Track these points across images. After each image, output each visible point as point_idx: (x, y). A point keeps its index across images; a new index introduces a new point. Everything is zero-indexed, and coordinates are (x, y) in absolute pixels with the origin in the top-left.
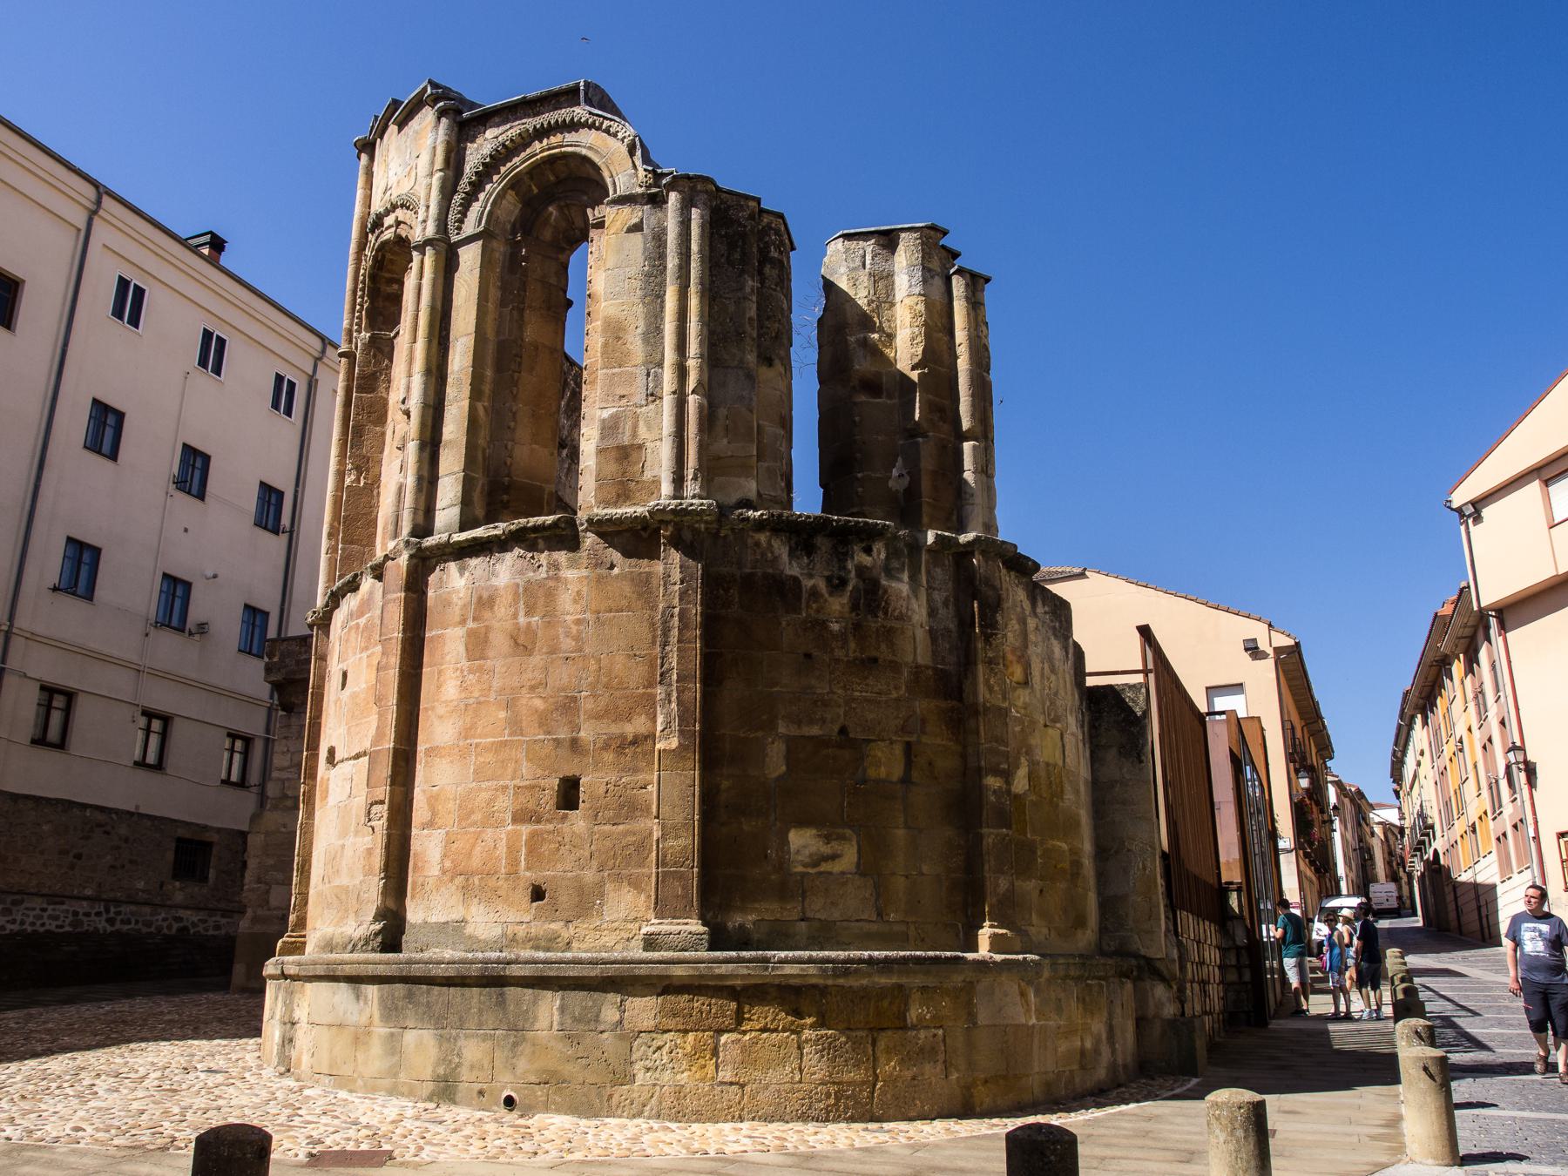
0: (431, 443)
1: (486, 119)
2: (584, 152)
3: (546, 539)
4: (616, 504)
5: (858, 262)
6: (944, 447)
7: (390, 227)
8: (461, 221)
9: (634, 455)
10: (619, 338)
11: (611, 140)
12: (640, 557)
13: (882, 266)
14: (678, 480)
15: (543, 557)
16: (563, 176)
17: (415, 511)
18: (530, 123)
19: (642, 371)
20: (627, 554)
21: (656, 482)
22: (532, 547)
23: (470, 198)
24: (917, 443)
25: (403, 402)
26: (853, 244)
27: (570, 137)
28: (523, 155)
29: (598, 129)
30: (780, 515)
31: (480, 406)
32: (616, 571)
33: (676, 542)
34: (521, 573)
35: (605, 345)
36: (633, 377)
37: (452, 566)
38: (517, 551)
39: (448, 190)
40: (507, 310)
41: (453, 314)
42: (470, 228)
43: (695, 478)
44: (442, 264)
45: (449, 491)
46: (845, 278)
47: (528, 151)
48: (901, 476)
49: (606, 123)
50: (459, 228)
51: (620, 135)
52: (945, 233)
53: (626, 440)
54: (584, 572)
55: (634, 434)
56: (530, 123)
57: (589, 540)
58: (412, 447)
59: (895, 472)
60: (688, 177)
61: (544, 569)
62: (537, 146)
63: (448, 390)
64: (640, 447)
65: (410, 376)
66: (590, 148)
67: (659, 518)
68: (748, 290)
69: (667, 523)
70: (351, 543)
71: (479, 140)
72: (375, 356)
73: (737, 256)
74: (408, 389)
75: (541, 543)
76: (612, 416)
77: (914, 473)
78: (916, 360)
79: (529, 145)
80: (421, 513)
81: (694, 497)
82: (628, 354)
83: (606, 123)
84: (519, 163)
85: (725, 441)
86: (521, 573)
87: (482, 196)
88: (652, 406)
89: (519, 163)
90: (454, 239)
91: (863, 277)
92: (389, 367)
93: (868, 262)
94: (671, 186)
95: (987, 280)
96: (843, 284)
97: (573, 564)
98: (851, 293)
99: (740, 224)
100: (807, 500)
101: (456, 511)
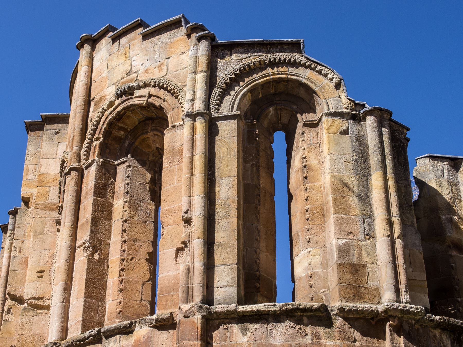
1: (231, 48)
2: (304, 81)
3: (309, 317)
4: (353, 300)
5: (440, 173)
8: (219, 105)
9: (361, 271)
10: (343, 197)
11: (322, 78)
12: (372, 337)
13: (452, 178)
14: (397, 291)
15: (308, 329)
18: (266, 57)
19: (359, 219)
20: (364, 334)
22: (299, 321)
23: (225, 93)
25: (186, 212)
26: (435, 162)
27: (292, 70)
28: (260, 74)
29: (312, 69)
30: (449, 321)
32: (357, 344)
33: (397, 330)
34: (292, 337)
35: (335, 199)
36: (354, 223)
37: (235, 328)
38: (288, 323)
39: (211, 83)
41: (217, 161)
42: (225, 110)
43: (406, 291)
46: (433, 181)
47: (264, 72)
49: (319, 68)
50: (218, 110)
51: (329, 76)
53: (355, 260)
54: (338, 343)
55: (360, 258)
56: (266, 57)
57: (339, 322)
60: (381, 110)
61: (309, 337)
62: (269, 71)
63: (217, 209)
65: (190, 196)
66: (307, 79)
67: (389, 314)
69: (393, 317)
70: (91, 298)
71: (227, 59)
72: (105, 174)
74: (190, 204)
75: (306, 320)
76: (344, 244)
79: (265, 69)
81: (407, 302)
82: (350, 207)
83: (319, 68)
84: (258, 78)
86: (292, 337)
87: (232, 93)
88: (368, 242)
89: (258, 78)
90: (214, 115)
91: (446, 185)
92: (113, 183)
93: (446, 174)
94: (370, 113)
96: (433, 184)
97: (329, 337)
98: (439, 190)
99: (401, 142)
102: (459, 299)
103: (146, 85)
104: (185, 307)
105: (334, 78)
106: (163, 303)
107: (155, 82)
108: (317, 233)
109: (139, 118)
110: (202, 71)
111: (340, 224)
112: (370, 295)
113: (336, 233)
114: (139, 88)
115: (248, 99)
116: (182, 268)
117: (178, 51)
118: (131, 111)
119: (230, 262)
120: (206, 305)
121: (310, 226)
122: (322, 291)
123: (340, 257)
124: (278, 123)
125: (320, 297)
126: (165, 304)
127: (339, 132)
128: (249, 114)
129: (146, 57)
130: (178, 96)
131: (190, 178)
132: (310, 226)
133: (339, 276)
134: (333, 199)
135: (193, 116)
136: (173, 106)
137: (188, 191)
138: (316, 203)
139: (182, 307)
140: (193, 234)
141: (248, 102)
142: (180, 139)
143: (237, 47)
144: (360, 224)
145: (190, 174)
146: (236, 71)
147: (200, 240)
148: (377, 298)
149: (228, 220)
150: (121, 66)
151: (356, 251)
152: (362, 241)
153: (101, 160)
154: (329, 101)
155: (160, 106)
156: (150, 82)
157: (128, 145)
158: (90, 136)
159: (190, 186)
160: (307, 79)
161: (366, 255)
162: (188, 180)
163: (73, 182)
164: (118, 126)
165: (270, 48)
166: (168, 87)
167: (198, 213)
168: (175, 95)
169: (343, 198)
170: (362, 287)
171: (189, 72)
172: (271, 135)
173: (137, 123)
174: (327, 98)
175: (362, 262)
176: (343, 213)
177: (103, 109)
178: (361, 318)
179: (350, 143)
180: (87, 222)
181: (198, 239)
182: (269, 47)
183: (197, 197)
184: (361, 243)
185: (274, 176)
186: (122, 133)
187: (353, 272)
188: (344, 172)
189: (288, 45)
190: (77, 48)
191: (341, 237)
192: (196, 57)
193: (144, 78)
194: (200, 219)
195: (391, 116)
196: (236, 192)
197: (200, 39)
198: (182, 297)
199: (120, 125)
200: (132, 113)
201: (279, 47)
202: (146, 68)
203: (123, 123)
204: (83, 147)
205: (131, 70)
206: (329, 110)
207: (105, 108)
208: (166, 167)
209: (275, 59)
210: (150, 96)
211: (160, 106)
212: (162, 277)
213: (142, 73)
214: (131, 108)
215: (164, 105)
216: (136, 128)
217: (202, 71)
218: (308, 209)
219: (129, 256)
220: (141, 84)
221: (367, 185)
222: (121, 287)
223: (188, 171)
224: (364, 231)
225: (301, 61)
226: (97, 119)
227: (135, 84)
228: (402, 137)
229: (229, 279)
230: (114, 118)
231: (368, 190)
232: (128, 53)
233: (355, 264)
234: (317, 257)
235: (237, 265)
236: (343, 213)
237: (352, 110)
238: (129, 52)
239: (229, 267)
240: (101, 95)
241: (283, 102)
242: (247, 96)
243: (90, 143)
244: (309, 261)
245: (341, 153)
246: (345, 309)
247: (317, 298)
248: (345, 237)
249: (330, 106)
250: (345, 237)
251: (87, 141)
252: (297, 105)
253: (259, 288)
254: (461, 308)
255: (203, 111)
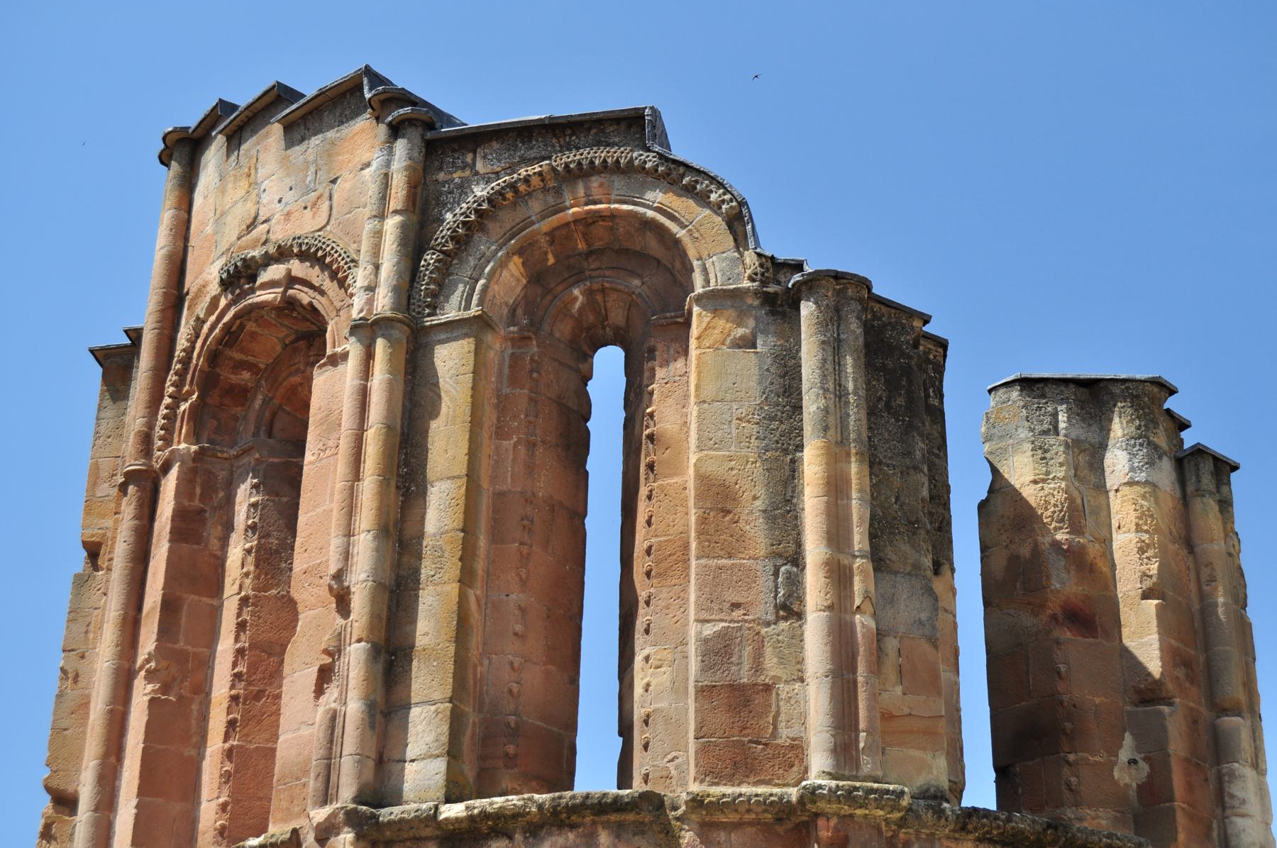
0: (392, 656)
4: (730, 780)
6: (1195, 722)
7: (271, 284)
16: (598, 245)
17: (361, 758)
21: (797, 749)
24: (1160, 713)
31: (471, 593)
39: (415, 243)
40: (508, 444)
44: (402, 357)
45: (425, 729)
48: (1133, 762)
52: (1172, 392)
55: (758, 667)
58: (355, 656)
59: (1124, 755)
64: (768, 688)
65: (349, 533)
68: (918, 454)
73: (901, 401)
74: (347, 555)
77: (1156, 756)
78: (1148, 583)
80: (371, 764)
82: (742, 538)
85: (899, 690)
88: (783, 625)
93: (1062, 425)
95: (1235, 468)
99: (903, 354)
100: (981, 792)
101: (440, 765)
102: (1071, 757)
103: (282, 254)
104: (320, 814)
105: (723, 201)
106: (284, 804)
107: (300, 245)
108: (667, 607)
109: (281, 335)
110: (396, 212)
111: (713, 583)
112: (777, 761)
113: (699, 608)
114: (268, 260)
115: (517, 273)
116: (320, 715)
117: (357, 159)
118: (256, 321)
119: (437, 696)
120: (364, 808)
121: (652, 590)
122: (670, 757)
123: (706, 667)
124: (604, 327)
125: (664, 774)
126: (288, 809)
127: (728, 342)
128: (520, 311)
129: (290, 181)
130: (346, 277)
131: (352, 487)
132: (652, 590)
133: (699, 719)
134: (697, 520)
135: (367, 330)
136: (338, 305)
137: (343, 522)
138: (671, 531)
139: (312, 814)
140: (349, 630)
141: (518, 280)
142: (343, 394)
143: (490, 141)
144: (764, 582)
145: (350, 477)
146: (480, 205)
147: (363, 644)
148: (795, 769)
149: (439, 588)
150: (240, 204)
151: (748, 651)
152: (768, 624)
153: (194, 448)
154: (708, 264)
155: (311, 304)
156: (292, 246)
157: (261, 406)
158: (171, 389)
159: (350, 509)
160: (658, 210)
161: (775, 660)
162: (346, 494)
163: (132, 507)
164: (231, 358)
165: (571, 136)
166: (324, 256)
167: (363, 576)
168: (340, 275)
169: (724, 517)
170: (758, 743)
171: (368, 214)
172: (587, 357)
173: (279, 348)
174: (705, 256)
175: (763, 677)
176: (721, 553)
177: (198, 318)
178: (751, 824)
179: (755, 371)
180: (153, 609)
181: (359, 641)
182: (569, 132)
183: (363, 536)
184: (764, 630)
185: (588, 467)
186: (246, 375)
187: (739, 710)
188: (733, 448)
189: (618, 124)
190: (162, 162)
191: (713, 617)
192: (386, 175)
193: (281, 233)
194: (366, 592)
195: (869, 289)
196: (461, 516)
197: (396, 131)
198: (315, 790)
199: (238, 356)
200: (259, 326)
201: (593, 132)
202: (287, 209)
203: (243, 351)
204: (159, 417)
205: (256, 218)
206: (707, 281)
207: (202, 316)
208: (311, 463)
209: (579, 163)
210: (291, 280)
211: (311, 304)
212: (285, 741)
213: (278, 222)
214: (253, 315)
215: (320, 303)
216: (278, 361)
217: (396, 212)
218: (650, 547)
219: (251, 688)
220: (272, 249)
221: (794, 478)
222: (228, 767)
223: (348, 471)
224: (775, 597)
225: (645, 162)
226: (186, 344)
227: (256, 253)
228: (907, 342)
229: (429, 738)
230: (219, 341)
231: (793, 491)
232: (253, 171)
233: (744, 685)
234: (663, 669)
235: (450, 701)
236: (721, 553)
237: (764, 283)
238: (256, 169)
239: (433, 708)
240: (199, 281)
241: (607, 273)
242: (511, 266)
243: (173, 408)
244: (645, 681)
245: (729, 397)
246: (702, 802)
247: (658, 774)
248: (722, 616)
249: (712, 276)
250: (722, 616)
251: (167, 400)
252: (640, 276)
253: (516, 755)
254: (1073, 779)
255: (389, 314)
